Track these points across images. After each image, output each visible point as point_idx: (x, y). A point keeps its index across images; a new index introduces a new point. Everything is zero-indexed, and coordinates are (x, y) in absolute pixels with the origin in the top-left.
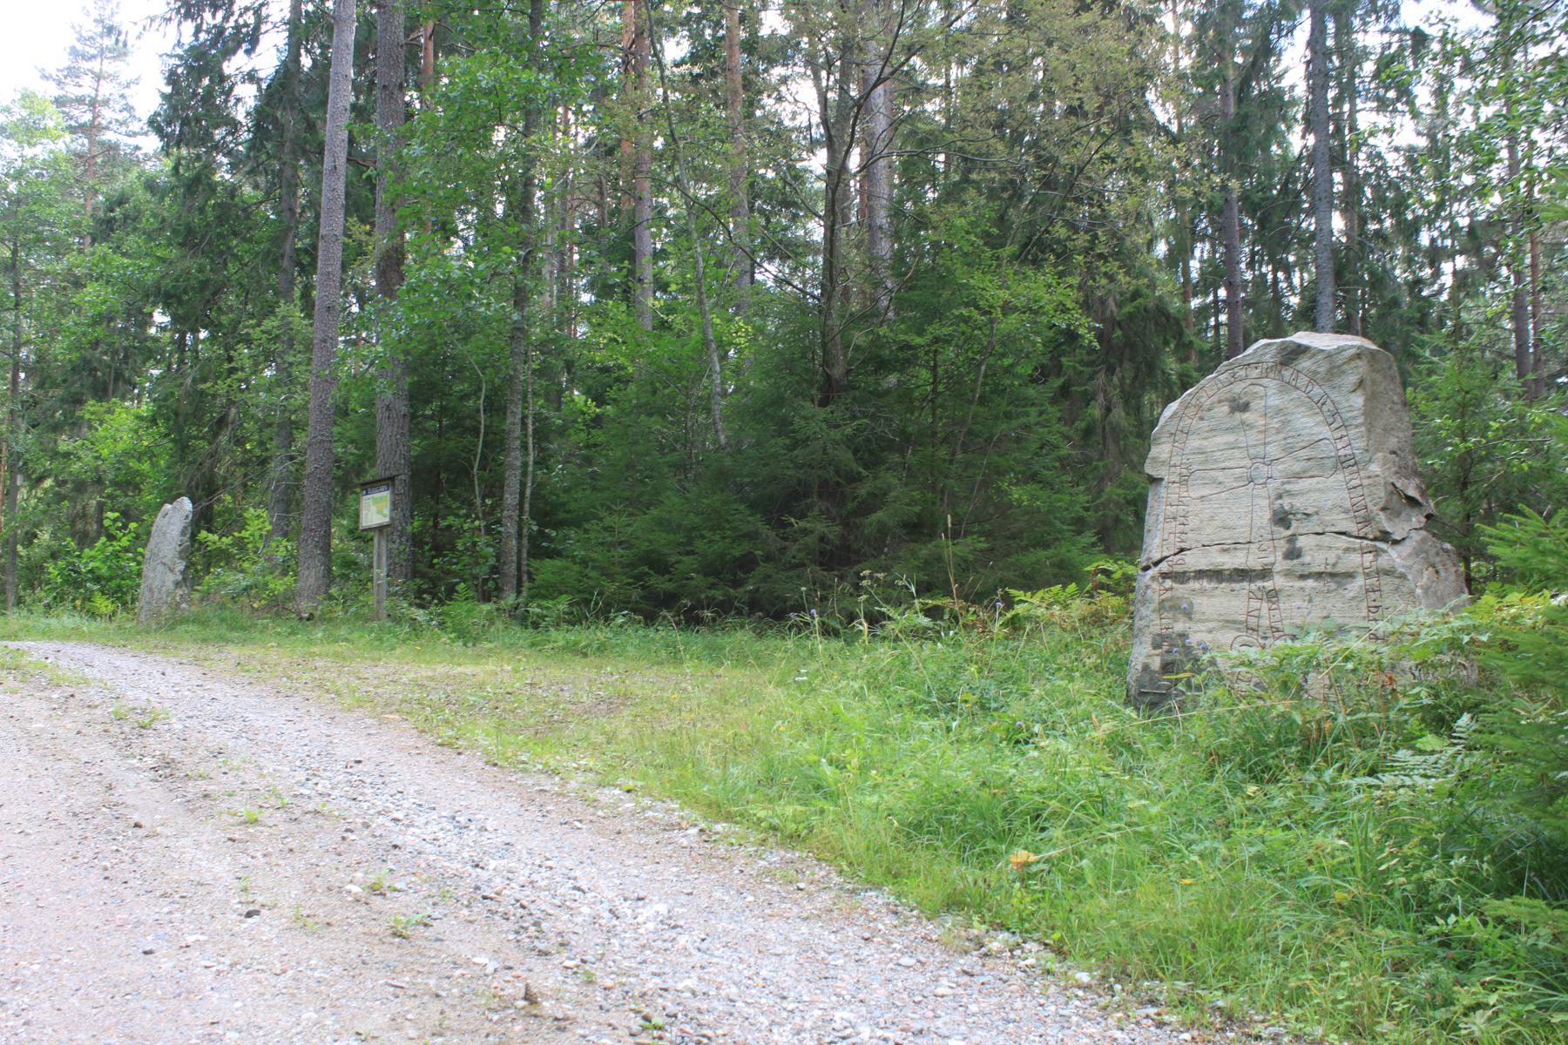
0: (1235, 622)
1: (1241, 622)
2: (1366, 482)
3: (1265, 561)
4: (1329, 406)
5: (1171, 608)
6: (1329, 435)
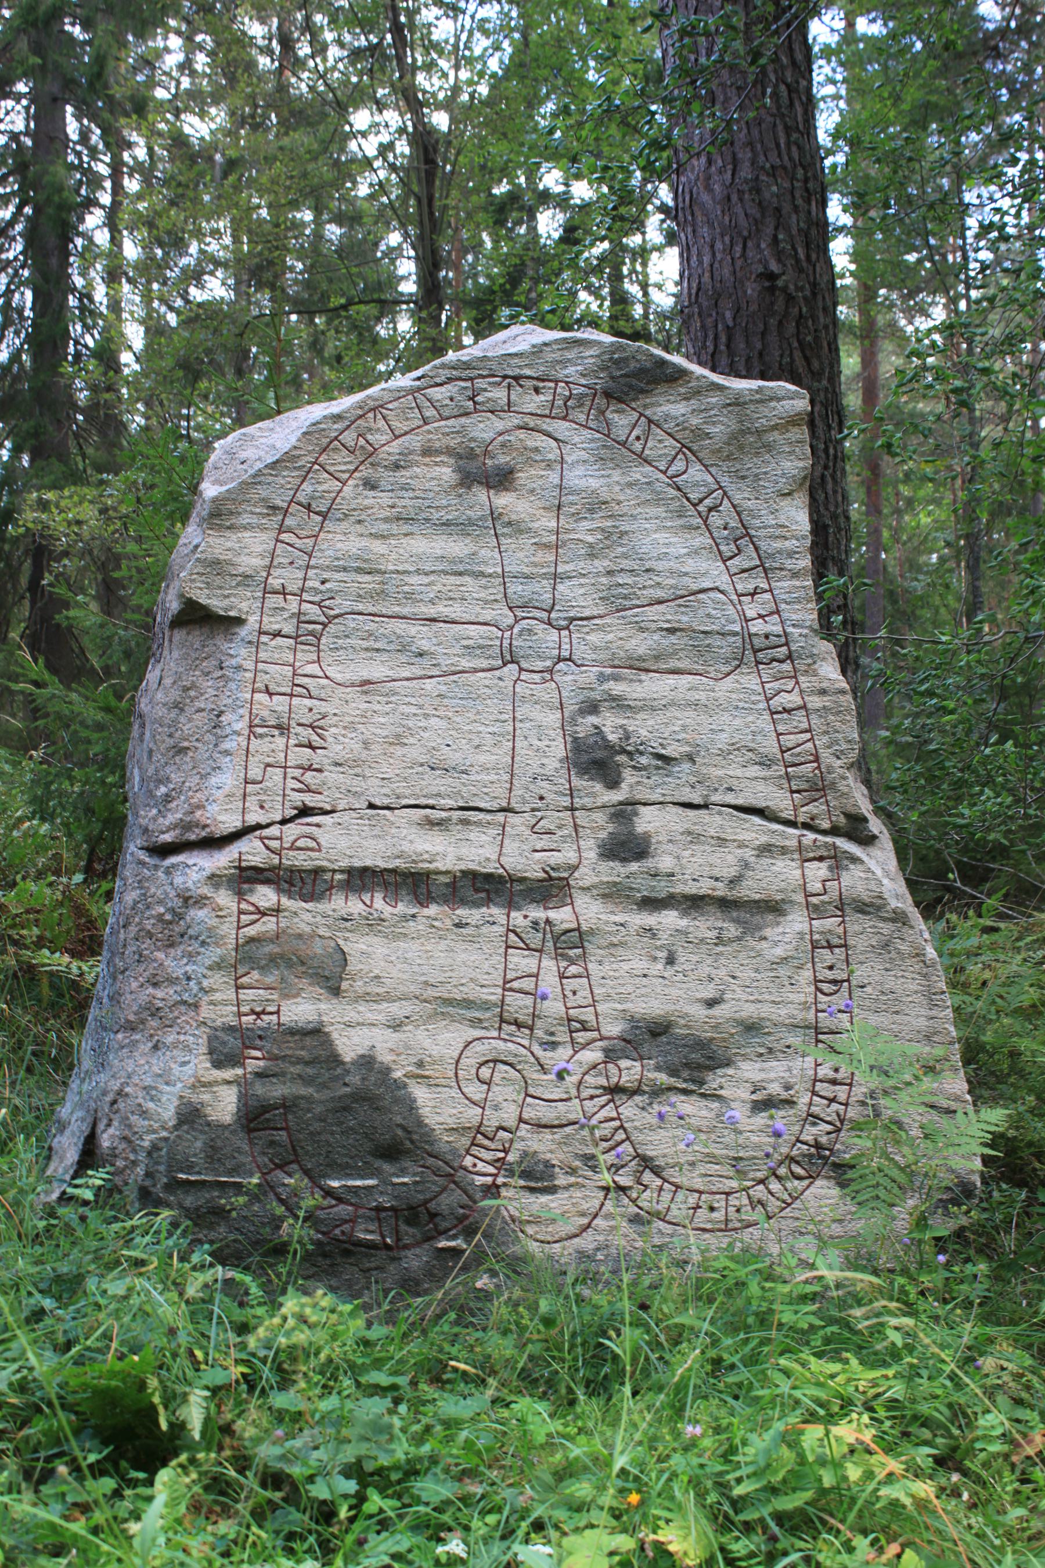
0: (468, 1004)
1: (486, 1006)
2: (815, 702)
3: (555, 858)
4: (726, 515)
5: (273, 960)
6: (723, 581)
